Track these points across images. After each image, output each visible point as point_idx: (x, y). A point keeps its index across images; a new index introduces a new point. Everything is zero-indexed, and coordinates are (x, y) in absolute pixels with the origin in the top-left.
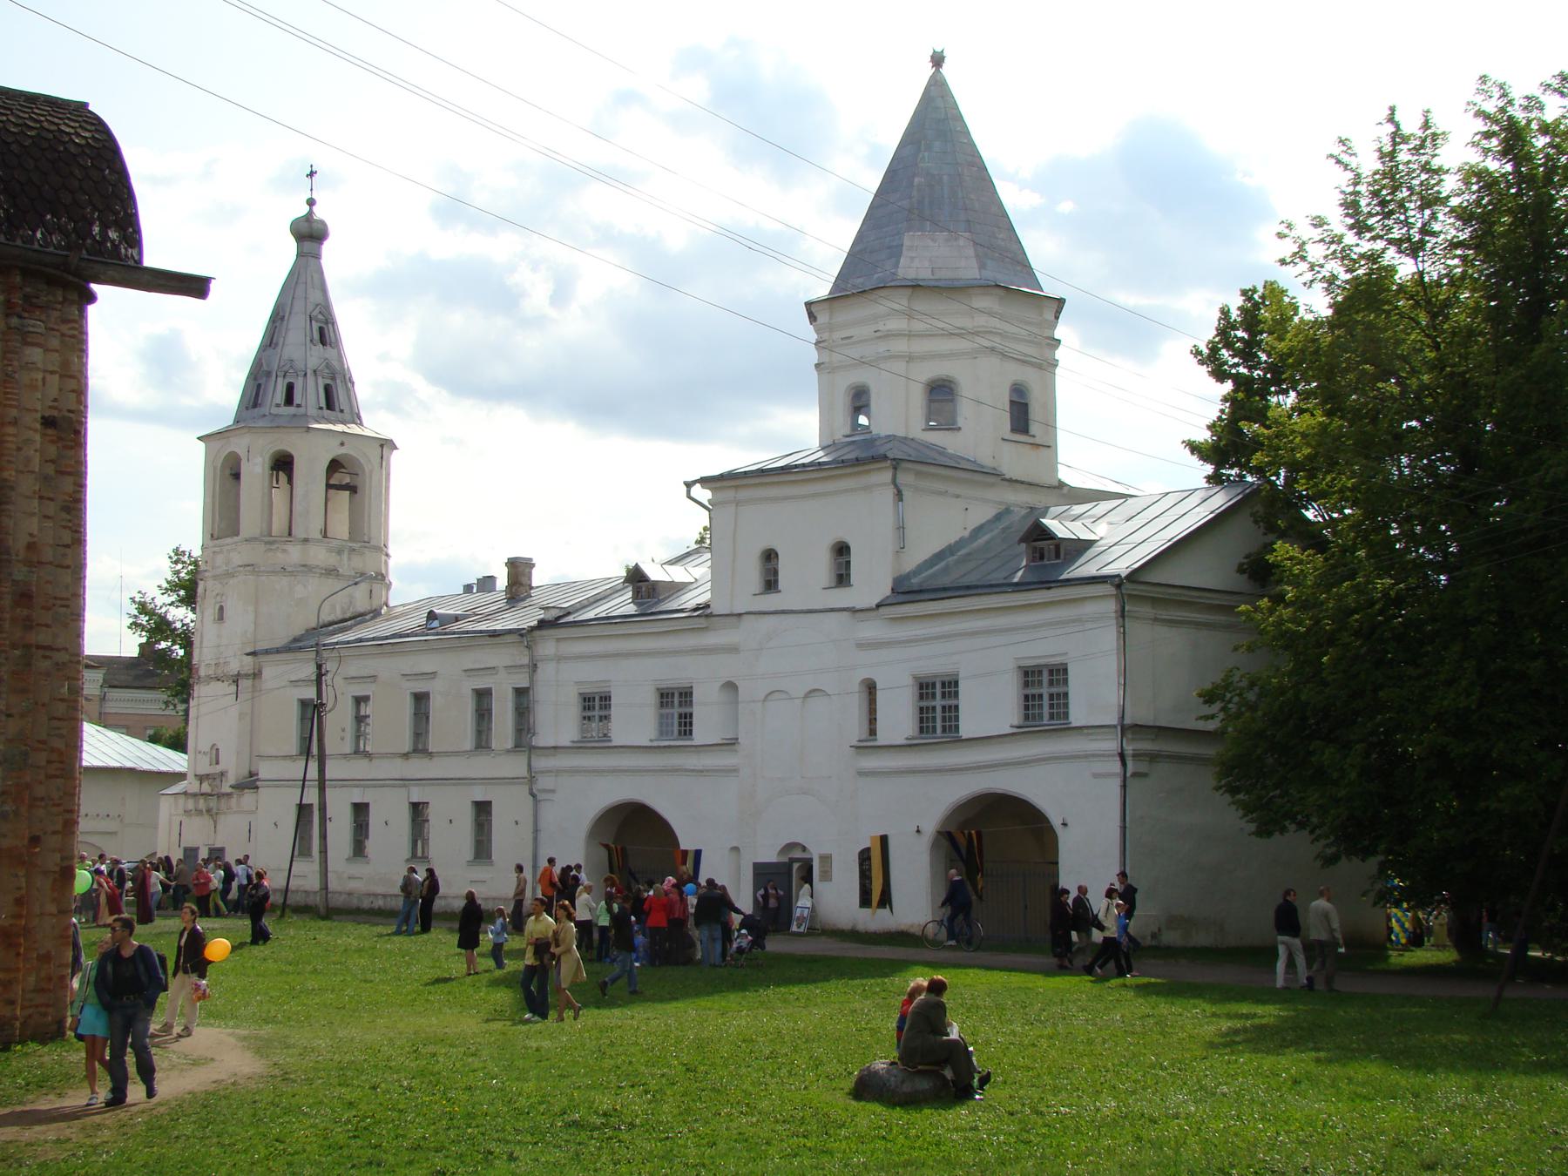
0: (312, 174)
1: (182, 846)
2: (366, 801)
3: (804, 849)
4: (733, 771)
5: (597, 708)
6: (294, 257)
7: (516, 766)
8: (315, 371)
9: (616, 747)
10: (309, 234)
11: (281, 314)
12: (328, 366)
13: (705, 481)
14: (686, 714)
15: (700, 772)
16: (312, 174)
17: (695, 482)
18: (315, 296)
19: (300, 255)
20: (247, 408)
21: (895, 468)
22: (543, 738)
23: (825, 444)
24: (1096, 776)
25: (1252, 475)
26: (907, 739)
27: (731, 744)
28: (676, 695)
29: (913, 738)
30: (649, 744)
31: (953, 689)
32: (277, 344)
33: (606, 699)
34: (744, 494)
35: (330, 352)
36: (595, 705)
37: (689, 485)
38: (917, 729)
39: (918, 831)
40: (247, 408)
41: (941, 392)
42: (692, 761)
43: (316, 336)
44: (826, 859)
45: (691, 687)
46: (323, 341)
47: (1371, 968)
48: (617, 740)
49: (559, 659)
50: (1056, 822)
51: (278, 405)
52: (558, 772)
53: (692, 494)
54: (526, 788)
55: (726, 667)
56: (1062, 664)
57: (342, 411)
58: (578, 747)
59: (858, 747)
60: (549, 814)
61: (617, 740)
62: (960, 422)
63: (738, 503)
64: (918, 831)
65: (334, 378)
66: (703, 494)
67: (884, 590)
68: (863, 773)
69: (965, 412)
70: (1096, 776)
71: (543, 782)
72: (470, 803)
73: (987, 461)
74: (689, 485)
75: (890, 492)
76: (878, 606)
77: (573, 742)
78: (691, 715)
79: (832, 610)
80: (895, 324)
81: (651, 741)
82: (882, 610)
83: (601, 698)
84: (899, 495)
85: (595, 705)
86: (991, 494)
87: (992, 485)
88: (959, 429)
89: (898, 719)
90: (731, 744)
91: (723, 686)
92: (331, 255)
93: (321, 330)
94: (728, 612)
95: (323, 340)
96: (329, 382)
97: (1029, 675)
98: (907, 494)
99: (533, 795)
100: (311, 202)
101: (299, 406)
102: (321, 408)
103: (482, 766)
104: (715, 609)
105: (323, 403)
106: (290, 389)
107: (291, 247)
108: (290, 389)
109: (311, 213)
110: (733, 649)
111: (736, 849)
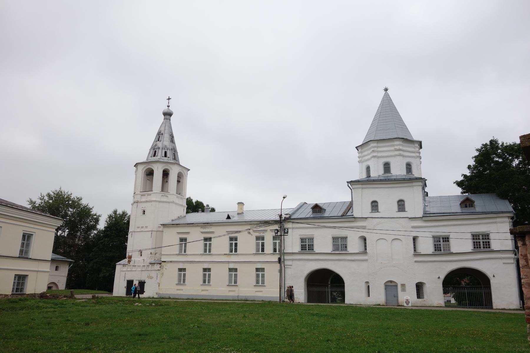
0: (169, 99)
2: (184, 268)
3: (391, 282)
4: (367, 260)
9: (315, 253)
22: (288, 250)
24: (504, 263)
25: (71, 209)
26: (432, 252)
28: (307, 240)
38: (434, 250)
41: (387, 167)
44: (403, 285)
45: (347, 237)
48: (453, 250)
49: (293, 228)
51: (163, 157)
52: (293, 260)
59: (414, 255)
64: (439, 278)
68: (416, 262)
70: (504, 263)
72: (255, 269)
74: (348, 182)
77: (299, 251)
79: (404, 218)
80: (401, 147)
81: (332, 251)
82: (423, 218)
91: (360, 237)
94: (361, 217)
96: (174, 152)
97: (335, 239)
100: (168, 106)
101: (169, 157)
102: (163, 157)
105: (163, 155)
106: (166, 153)
107: (384, 92)
108: (166, 153)
110: (364, 228)
111: (367, 282)
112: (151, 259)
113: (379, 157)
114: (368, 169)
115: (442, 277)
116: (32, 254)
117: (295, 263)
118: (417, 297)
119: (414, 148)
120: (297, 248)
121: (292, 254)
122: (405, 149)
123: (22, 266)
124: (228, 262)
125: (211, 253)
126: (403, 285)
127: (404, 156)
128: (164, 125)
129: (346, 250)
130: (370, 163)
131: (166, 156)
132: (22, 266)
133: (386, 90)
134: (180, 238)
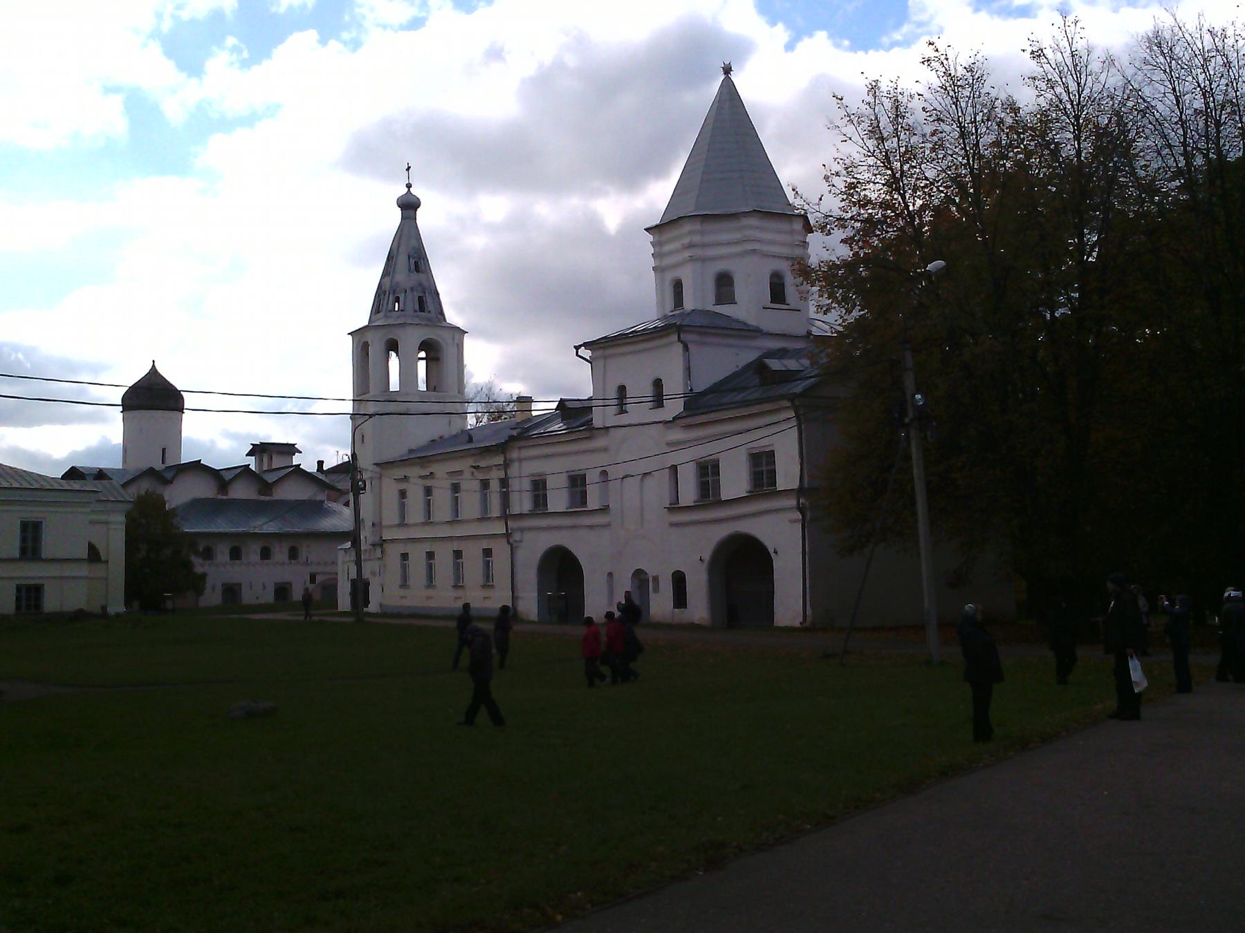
1: (350, 579)
4: (607, 526)
6: (400, 220)
7: (499, 528)
8: (412, 288)
11: (689, 258)
12: (420, 284)
13: (586, 345)
15: (591, 527)
17: (580, 346)
18: (414, 243)
23: (660, 317)
27: (605, 509)
34: (609, 351)
36: (539, 487)
37: (577, 348)
41: (724, 284)
42: (587, 521)
43: (413, 267)
44: (656, 579)
47: (339, 548)
50: (771, 551)
51: (416, 311)
52: (522, 530)
55: (601, 460)
57: (430, 312)
58: (531, 515)
60: (521, 554)
61: (551, 509)
63: (605, 358)
68: (672, 525)
69: (741, 290)
71: (517, 536)
73: (753, 322)
74: (577, 348)
75: (680, 346)
80: (697, 239)
84: (686, 348)
90: (605, 509)
92: (423, 218)
93: (416, 263)
95: (417, 269)
98: (691, 347)
99: (511, 545)
100: (409, 186)
102: (416, 311)
110: (605, 450)
113: (704, 260)
114: (678, 286)
115: (707, 556)
116: (46, 552)
117: (528, 536)
119: (792, 232)
122: (708, 239)
123: (31, 572)
125: (546, 511)
127: (704, 260)
128: (239, 470)
129: (584, 503)
130: (687, 275)
131: (422, 309)
132: (31, 572)
133: (154, 361)
134: (290, 584)
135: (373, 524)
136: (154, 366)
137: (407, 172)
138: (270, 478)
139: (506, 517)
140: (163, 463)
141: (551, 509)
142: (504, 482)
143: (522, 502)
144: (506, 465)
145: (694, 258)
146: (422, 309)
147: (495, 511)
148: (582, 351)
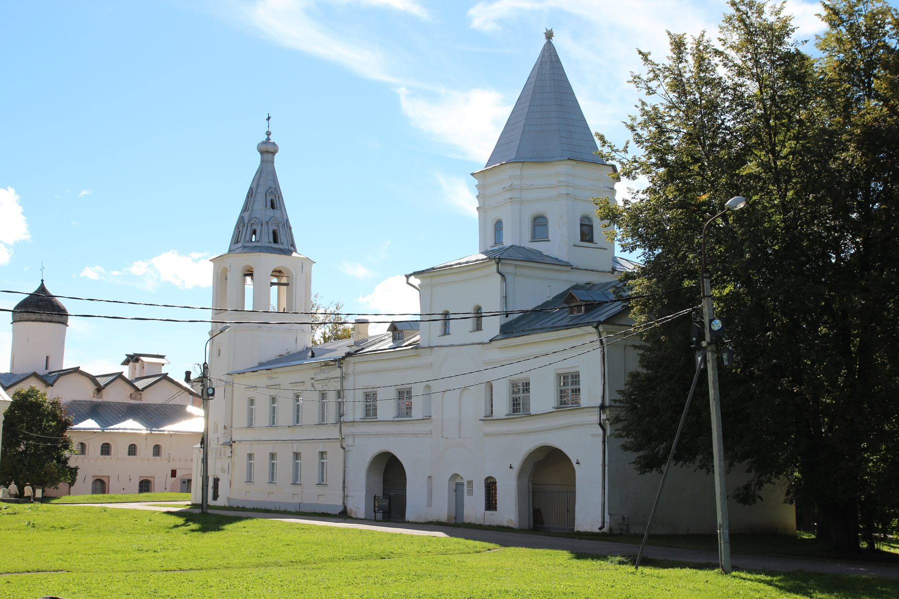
0: (269, 119)
5: (570, 384)
10: (268, 151)
13: (416, 274)
14: (576, 389)
16: (269, 119)
17: (411, 275)
19: (262, 161)
20: (234, 244)
21: (498, 263)
22: (348, 417)
27: (428, 418)
29: (509, 415)
30: (392, 419)
31: (528, 387)
32: (248, 209)
33: (409, 392)
35: (277, 213)
36: (370, 398)
37: (407, 277)
38: (512, 410)
39: (511, 467)
40: (234, 244)
44: (470, 483)
46: (273, 207)
52: (354, 436)
53: (410, 282)
54: (339, 445)
56: (576, 372)
57: (282, 243)
58: (362, 421)
62: (550, 238)
65: (278, 226)
66: (415, 281)
67: (496, 332)
68: (486, 435)
71: (349, 441)
72: (318, 453)
73: (564, 258)
74: (407, 277)
76: (491, 341)
77: (361, 419)
78: (579, 389)
82: (493, 343)
83: (573, 376)
85: (370, 398)
86: (564, 276)
87: (567, 271)
88: (549, 241)
89: (502, 406)
91: (425, 386)
92: (280, 162)
95: (273, 207)
96: (275, 228)
99: (343, 448)
100: (268, 134)
103: (298, 434)
104: (422, 344)
105: (271, 239)
109: (268, 139)
112: (226, 437)
115: (517, 465)
118: (486, 507)
120: (359, 413)
121: (350, 424)
124: (291, 440)
126: (470, 483)
131: (275, 241)
135: (225, 427)
136: (42, 284)
137: (267, 122)
138: (140, 384)
139: (340, 421)
140: (46, 369)
141: (380, 416)
142: (339, 394)
143: (354, 410)
144: (343, 378)
145: (513, 200)
146: (275, 241)
147: (331, 417)
148: (412, 280)
